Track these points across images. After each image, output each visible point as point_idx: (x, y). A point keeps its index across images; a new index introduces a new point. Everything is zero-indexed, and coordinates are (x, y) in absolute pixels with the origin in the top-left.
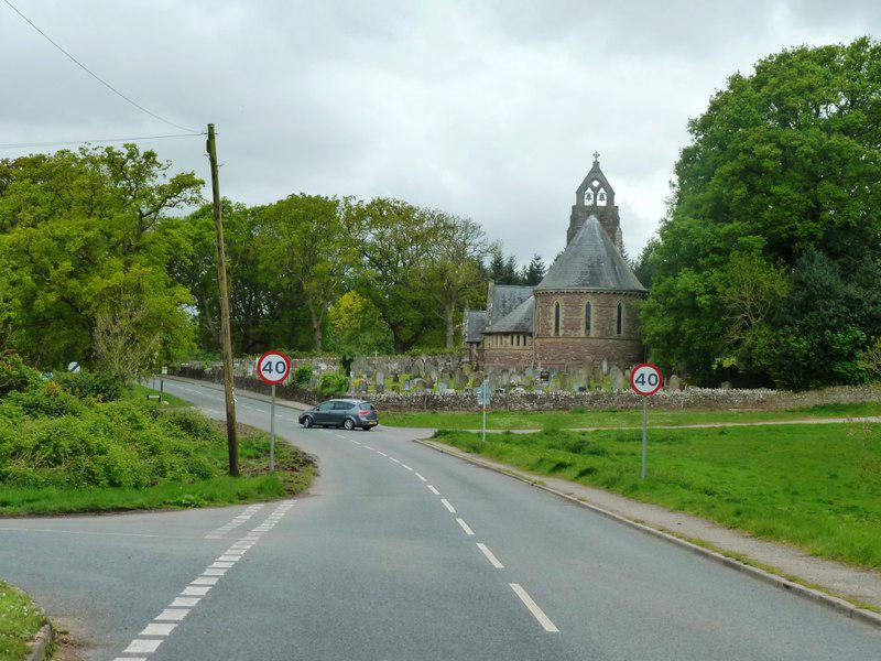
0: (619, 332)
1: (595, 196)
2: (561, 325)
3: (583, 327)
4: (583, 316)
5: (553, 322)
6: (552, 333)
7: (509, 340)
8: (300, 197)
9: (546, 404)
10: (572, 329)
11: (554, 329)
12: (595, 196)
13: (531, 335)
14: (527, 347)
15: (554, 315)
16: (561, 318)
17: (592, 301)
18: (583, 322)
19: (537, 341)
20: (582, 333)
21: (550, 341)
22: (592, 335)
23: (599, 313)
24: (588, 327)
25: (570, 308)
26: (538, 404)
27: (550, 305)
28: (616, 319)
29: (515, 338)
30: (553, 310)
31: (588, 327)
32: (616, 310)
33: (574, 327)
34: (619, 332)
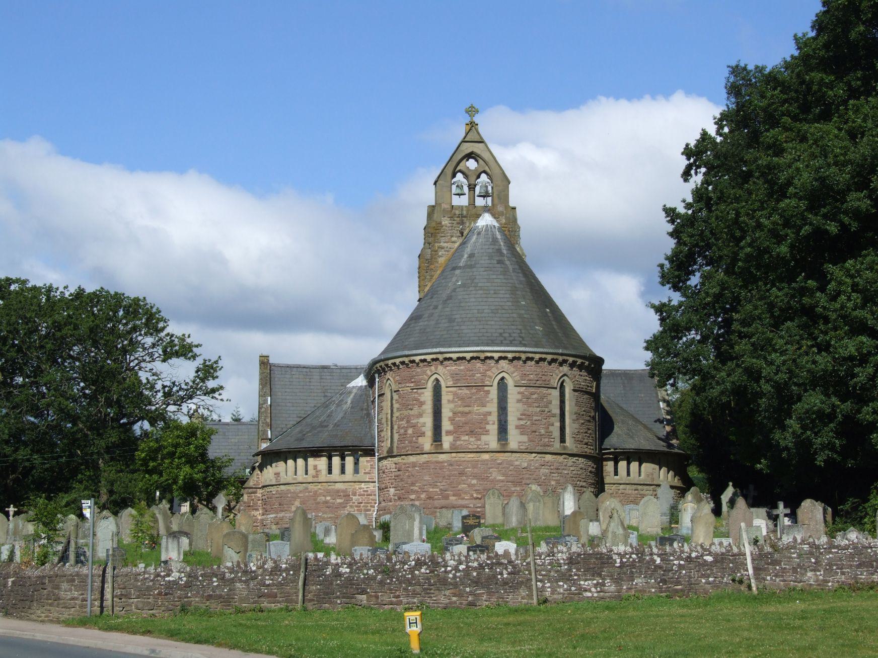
0: (563, 440)
1: (472, 188)
2: (446, 425)
3: (493, 428)
4: (493, 407)
5: (427, 421)
6: (427, 443)
7: (322, 462)
8: (697, 179)
9: (639, 581)
10: (471, 433)
11: (429, 433)
12: (472, 188)
13: (369, 452)
14: (361, 476)
15: (428, 407)
16: (446, 413)
17: (512, 375)
18: (494, 418)
19: (388, 463)
20: (491, 440)
21: (425, 457)
22: (513, 444)
23: (525, 400)
24: (503, 430)
25: (466, 391)
26: (617, 581)
27: (421, 387)
28: (557, 411)
29: (336, 460)
30: (427, 396)
31: (503, 430)
32: (556, 393)
33: (476, 429)
34: (563, 440)
